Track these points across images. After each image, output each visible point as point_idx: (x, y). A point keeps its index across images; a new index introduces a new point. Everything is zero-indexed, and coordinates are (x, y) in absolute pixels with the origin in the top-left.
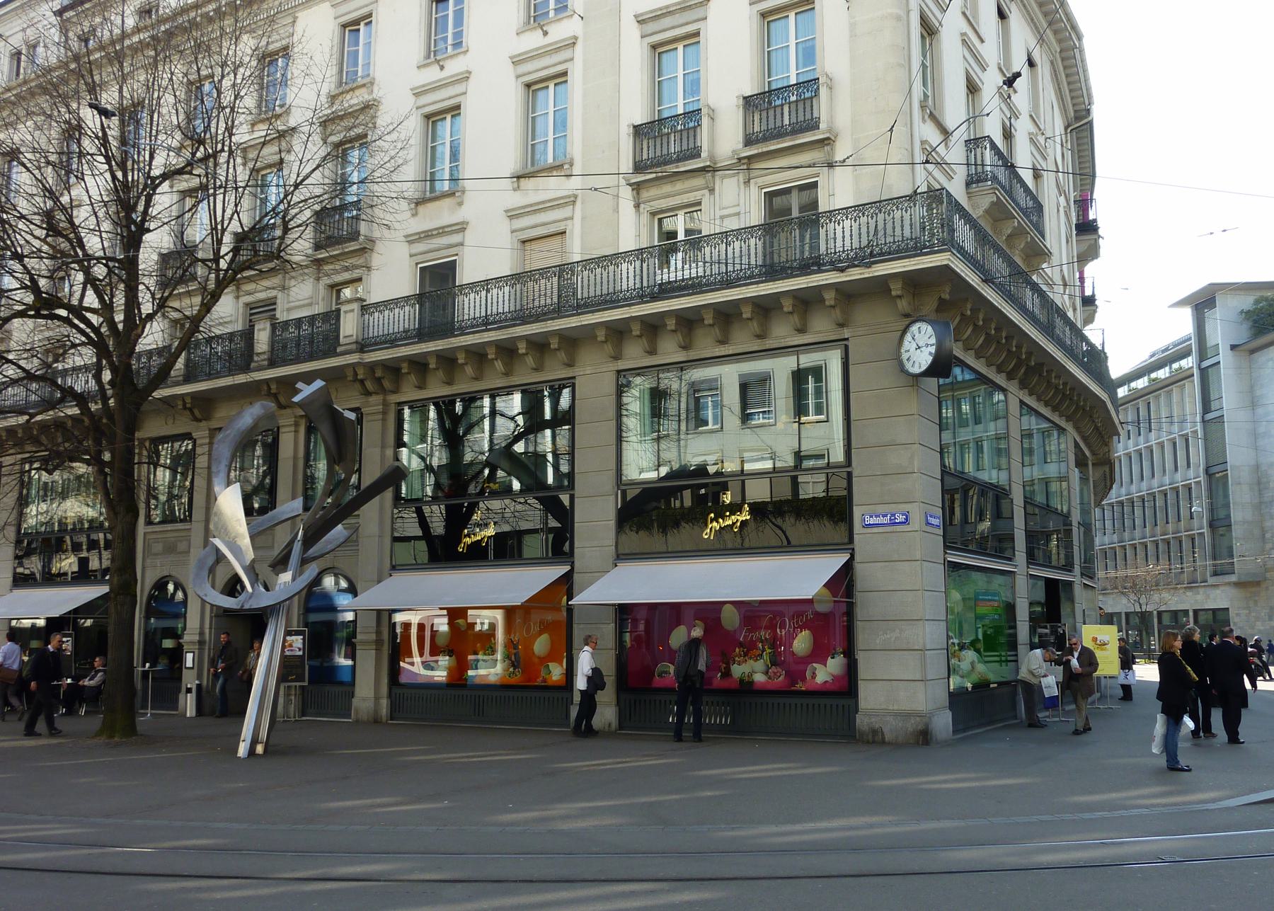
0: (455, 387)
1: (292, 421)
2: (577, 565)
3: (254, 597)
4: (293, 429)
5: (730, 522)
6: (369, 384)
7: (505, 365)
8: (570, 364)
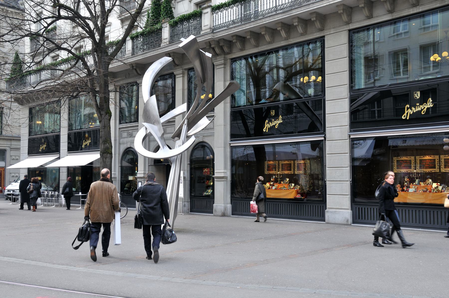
0: (260, 48)
1: (181, 71)
2: (327, 136)
3: (163, 153)
4: (181, 75)
5: (420, 109)
6: (217, 51)
7: (286, 33)
8: (322, 30)
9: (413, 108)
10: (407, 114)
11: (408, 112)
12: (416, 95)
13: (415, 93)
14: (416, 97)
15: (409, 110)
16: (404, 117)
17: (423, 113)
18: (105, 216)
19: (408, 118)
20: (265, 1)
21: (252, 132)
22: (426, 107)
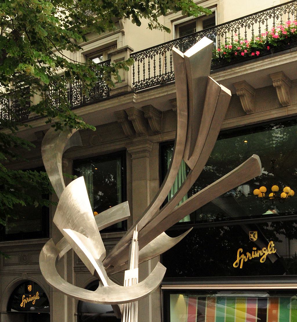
5: (257, 255)
9: (248, 254)
10: (240, 261)
11: (240, 260)
12: (252, 235)
13: (251, 233)
14: (252, 239)
15: (243, 256)
16: (236, 265)
17: (261, 261)
18: (219, 54)
19: (241, 267)
20: (132, 320)
21: (66, 298)
22: (266, 253)
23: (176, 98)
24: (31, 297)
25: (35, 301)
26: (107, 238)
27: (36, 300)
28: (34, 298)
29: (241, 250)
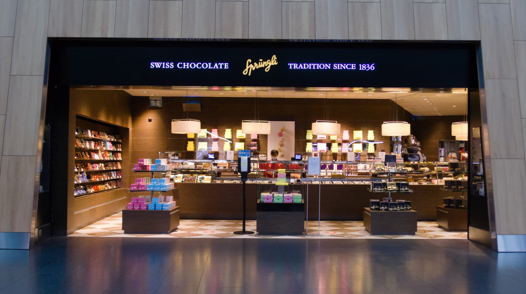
10: (249, 69)
15: (251, 66)
17: (266, 71)
19: (249, 75)
22: (270, 64)
23: (163, 98)
24: (262, 62)
25: (269, 67)
26: (80, 182)
27: (272, 66)
28: (268, 63)
29: (250, 60)
